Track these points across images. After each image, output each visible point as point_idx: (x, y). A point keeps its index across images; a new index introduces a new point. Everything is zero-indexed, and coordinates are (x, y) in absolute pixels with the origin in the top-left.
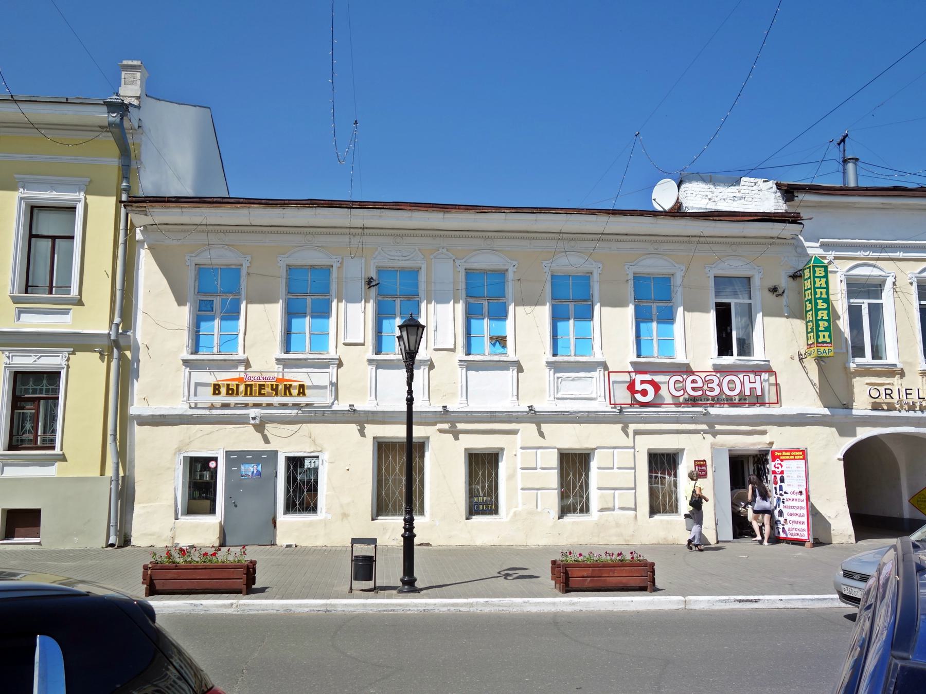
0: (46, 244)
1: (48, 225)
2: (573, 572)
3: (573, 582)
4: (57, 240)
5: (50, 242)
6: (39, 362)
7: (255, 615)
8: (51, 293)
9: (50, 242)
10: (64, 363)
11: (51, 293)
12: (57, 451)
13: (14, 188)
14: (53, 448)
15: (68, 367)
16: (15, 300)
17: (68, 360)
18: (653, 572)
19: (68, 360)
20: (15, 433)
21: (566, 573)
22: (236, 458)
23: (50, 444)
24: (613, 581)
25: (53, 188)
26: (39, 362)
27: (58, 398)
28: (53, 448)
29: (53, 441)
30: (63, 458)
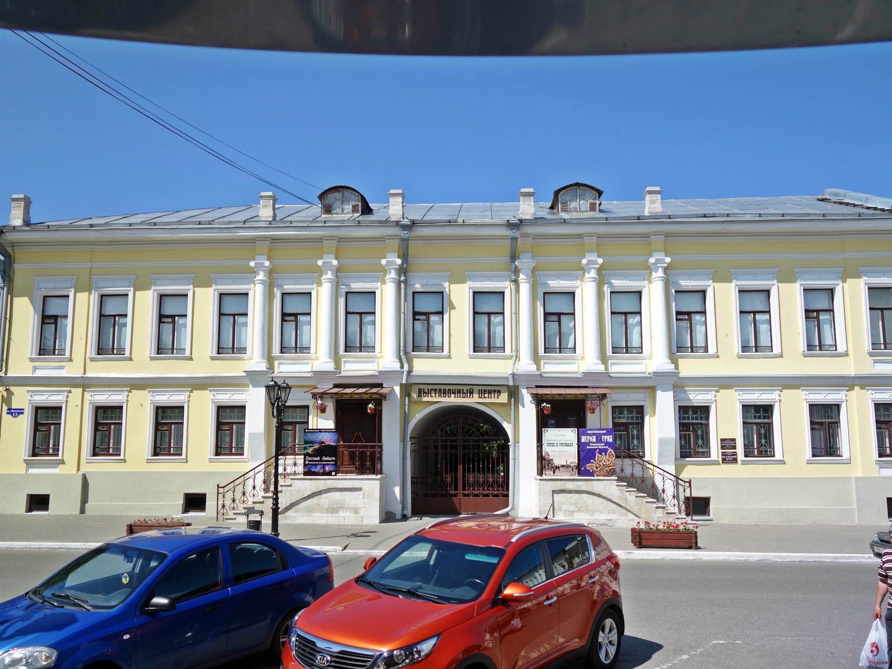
0: (485, 318)
1: (487, 305)
2: (644, 536)
3: (644, 542)
4: (885, 312)
5: (232, 318)
6: (50, 398)
7: (720, 562)
8: (173, 353)
9: (358, 316)
10: (187, 399)
11: (173, 353)
12: (60, 457)
13: (859, 277)
14: (119, 455)
15: (67, 401)
16: (871, 355)
17: (68, 397)
18: (696, 537)
19: (68, 397)
20: (158, 445)
21: (640, 536)
22: (735, 454)
23: (56, 452)
24: (665, 543)
25: (884, 276)
26: (50, 398)
27: (121, 424)
28: (119, 455)
29: (243, 448)
30: (124, 461)
